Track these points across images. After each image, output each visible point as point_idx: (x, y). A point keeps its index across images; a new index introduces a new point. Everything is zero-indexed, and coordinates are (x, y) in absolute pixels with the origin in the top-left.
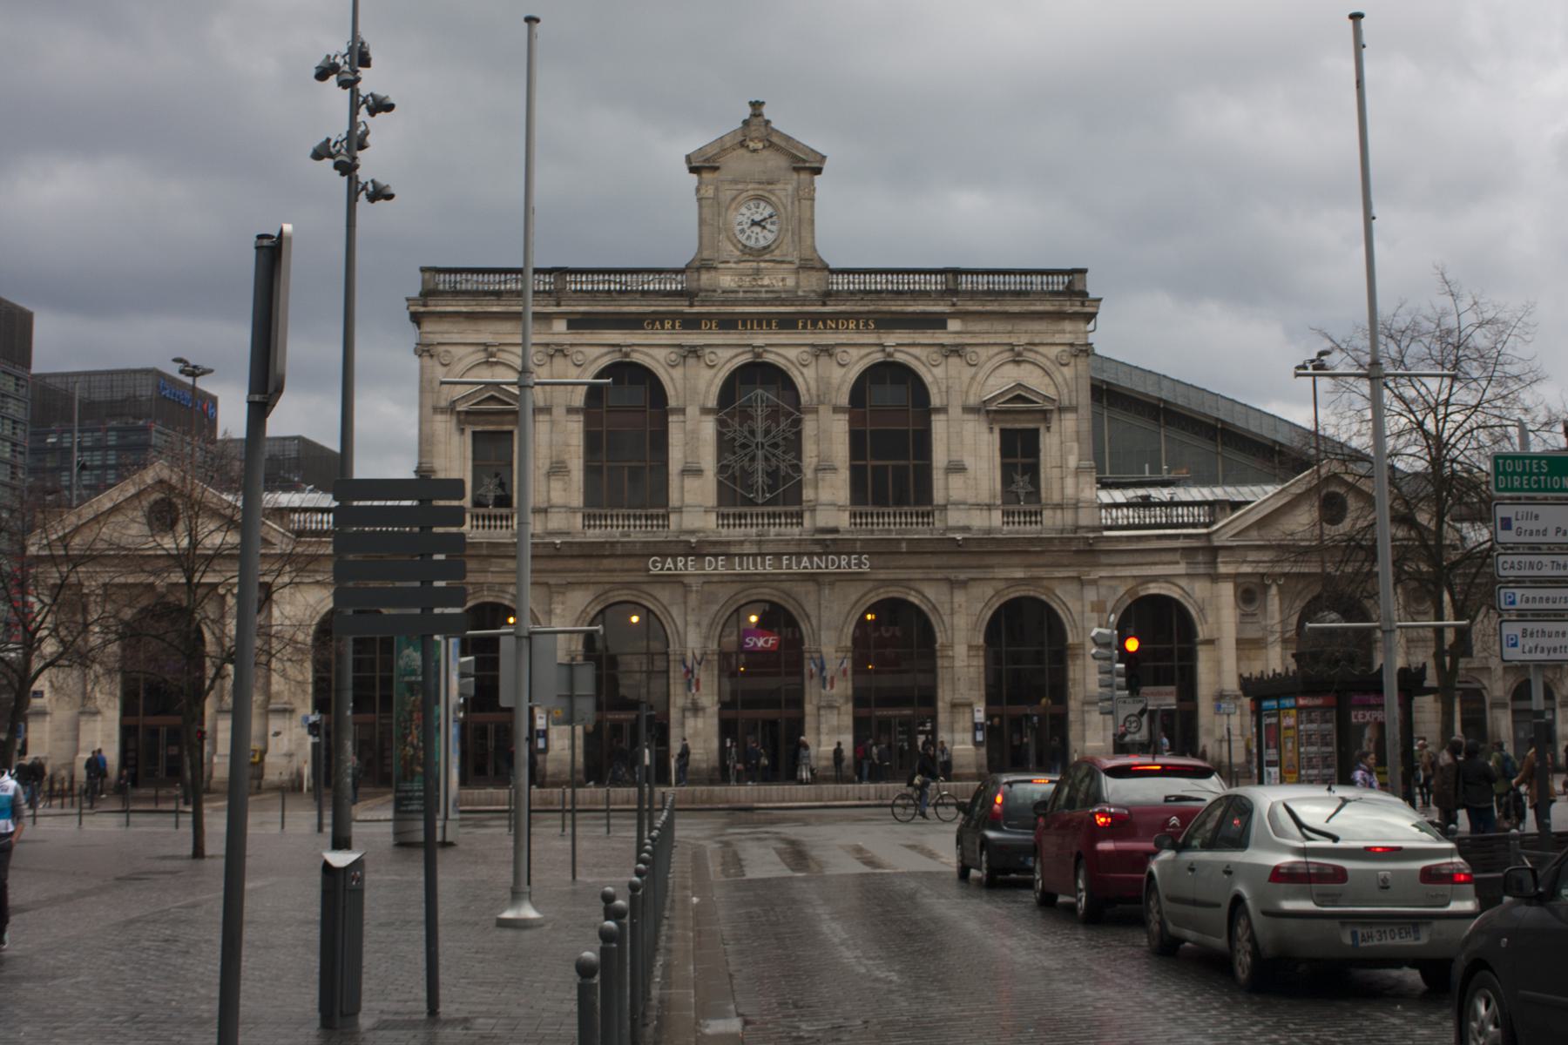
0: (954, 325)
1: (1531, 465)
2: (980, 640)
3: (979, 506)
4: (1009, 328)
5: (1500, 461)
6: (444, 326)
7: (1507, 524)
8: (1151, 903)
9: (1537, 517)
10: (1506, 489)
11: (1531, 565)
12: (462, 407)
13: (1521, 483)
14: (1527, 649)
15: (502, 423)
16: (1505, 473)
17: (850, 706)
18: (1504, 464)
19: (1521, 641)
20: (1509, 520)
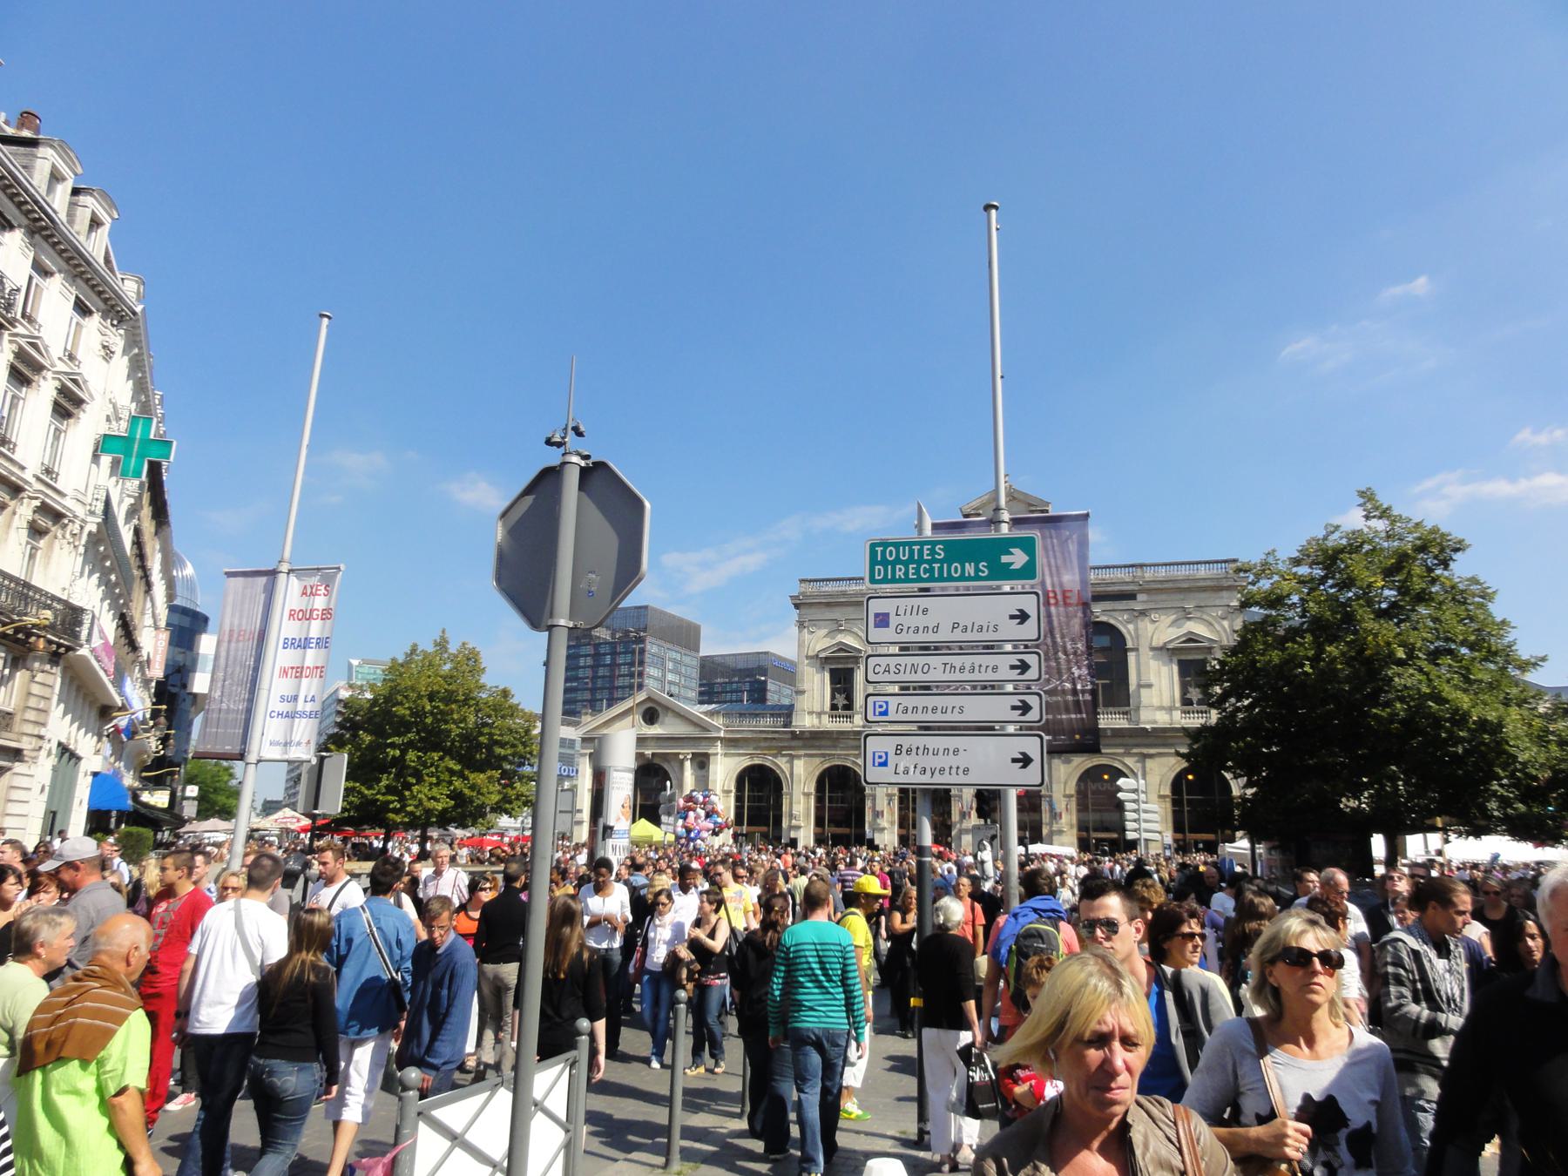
0: (1140, 597)
1: (921, 552)
2: (1167, 791)
3: (1161, 708)
4: (1182, 597)
5: (879, 549)
6: (813, 610)
7: (883, 620)
8: (605, 1005)
9: (925, 611)
10: (885, 580)
11: (914, 668)
12: (823, 655)
13: (906, 573)
14: (901, 769)
15: (847, 663)
16: (885, 563)
17: (1075, 831)
18: (883, 553)
19: (892, 760)
20: (887, 615)
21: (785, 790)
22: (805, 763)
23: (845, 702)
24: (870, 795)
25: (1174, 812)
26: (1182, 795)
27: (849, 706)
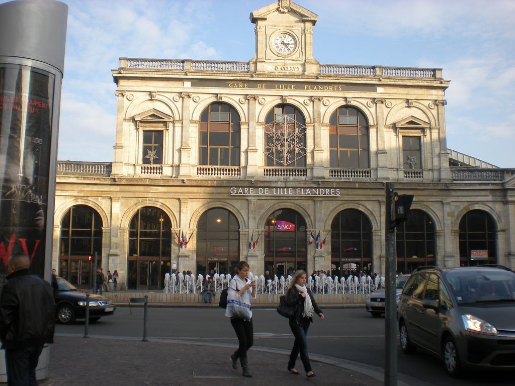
3: (392, 169)
21: (374, 228)
22: (122, 204)
23: (156, 157)
24: (503, 231)
25: (461, 243)
26: (465, 231)
27: (159, 160)
